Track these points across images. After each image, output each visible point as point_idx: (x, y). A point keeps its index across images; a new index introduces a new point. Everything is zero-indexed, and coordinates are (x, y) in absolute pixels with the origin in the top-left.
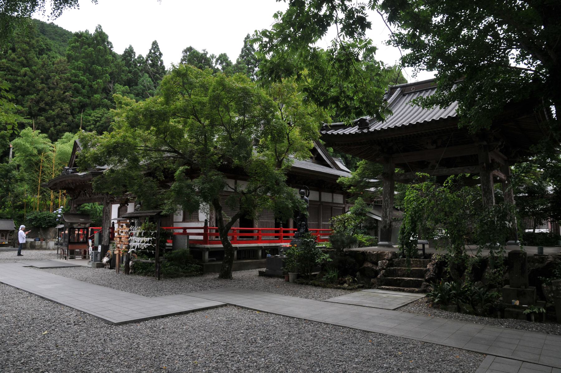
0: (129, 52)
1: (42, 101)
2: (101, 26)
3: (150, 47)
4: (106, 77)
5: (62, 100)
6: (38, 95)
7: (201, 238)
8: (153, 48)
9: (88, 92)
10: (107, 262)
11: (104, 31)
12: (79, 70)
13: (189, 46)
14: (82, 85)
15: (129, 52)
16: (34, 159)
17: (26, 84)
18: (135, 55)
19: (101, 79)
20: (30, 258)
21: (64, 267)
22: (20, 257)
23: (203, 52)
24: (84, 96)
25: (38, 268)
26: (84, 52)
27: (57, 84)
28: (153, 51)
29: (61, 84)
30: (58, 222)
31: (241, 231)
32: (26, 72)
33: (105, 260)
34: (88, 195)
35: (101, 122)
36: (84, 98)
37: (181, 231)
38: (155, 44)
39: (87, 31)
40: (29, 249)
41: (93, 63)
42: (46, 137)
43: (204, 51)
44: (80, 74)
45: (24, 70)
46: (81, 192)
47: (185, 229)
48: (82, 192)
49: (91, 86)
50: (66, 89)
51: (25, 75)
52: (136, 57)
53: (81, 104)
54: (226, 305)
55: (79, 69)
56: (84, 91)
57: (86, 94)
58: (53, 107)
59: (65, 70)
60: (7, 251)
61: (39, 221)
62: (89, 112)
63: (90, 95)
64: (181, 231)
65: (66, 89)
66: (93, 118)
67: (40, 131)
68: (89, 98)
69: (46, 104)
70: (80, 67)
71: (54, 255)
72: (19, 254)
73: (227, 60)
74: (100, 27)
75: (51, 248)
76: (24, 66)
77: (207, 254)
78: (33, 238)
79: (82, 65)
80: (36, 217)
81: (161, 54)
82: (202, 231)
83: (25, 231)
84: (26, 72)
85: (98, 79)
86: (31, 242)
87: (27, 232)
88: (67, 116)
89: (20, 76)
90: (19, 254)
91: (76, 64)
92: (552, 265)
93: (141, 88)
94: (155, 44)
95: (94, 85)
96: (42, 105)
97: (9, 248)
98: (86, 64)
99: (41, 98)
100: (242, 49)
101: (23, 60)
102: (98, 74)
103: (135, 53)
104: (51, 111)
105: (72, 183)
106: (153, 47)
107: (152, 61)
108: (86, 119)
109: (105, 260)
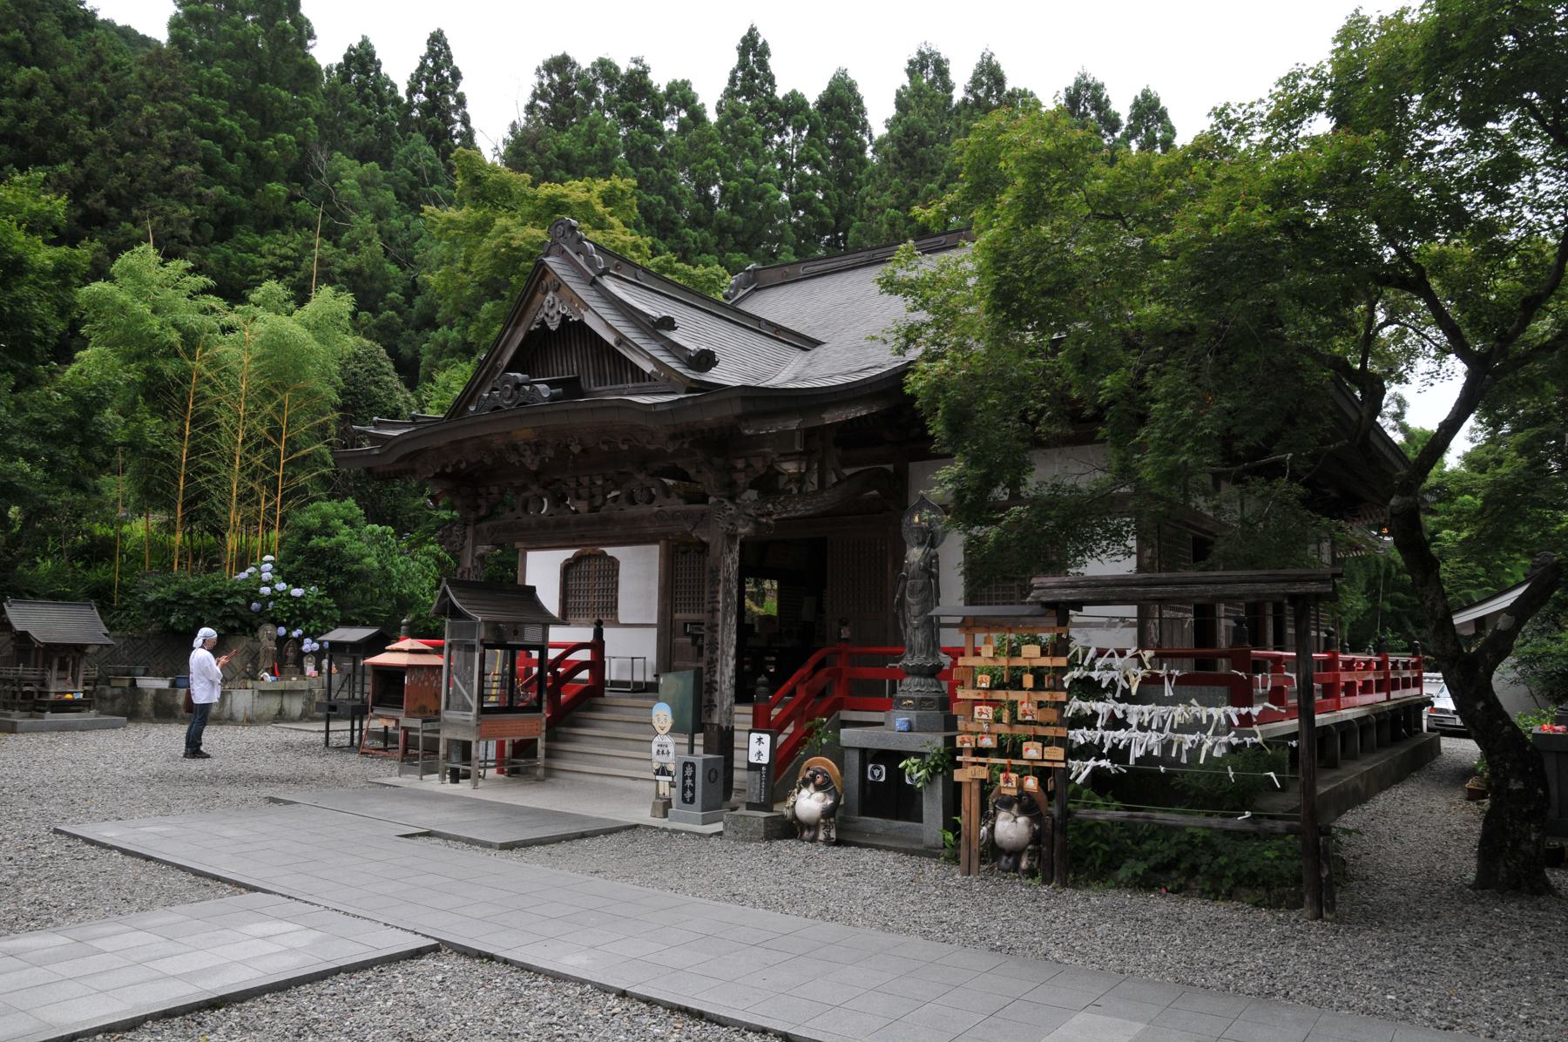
0: (362, 59)
1: (98, 188)
3: (424, 50)
4: (306, 127)
5: (165, 189)
6: (79, 163)
8: (432, 53)
9: (244, 174)
12: (217, 96)
13: (559, 54)
14: (225, 148)
15: (362, 59)
16: (169, 368)
17: (33, 123)
19: (290, 131)
20: (239, 767)
21: (583, 836)
22: (195, 765)
24: (231, 185)
25: (489, 845)
26: (231, 37)
27: (150, 135)
28: (430, 63)
29: (164, 135)
30: (261, 613)
32: (34, 83)
35: (299, 275)
36: (232, 193)
38: (437, 39)
40: (149, 720)
41: (260, 77)
42: (206, 291)
44: (220, 111)
45: (24, 74)
49: (253, 156)
50: (178, 152)
51: (29, 92)
53: (222, 210)
54: (429, 834)
55: (216, 91)
56: (233, 167)
57: (237, 178)
58: (135, 211)
59: (175, 87)
60: (64, 728)
61: (193, 608)
62: (248, 240)
63: (252, 184)
65: (178, 152)
66: (270, 259)
67: (190, 264)
68: (249, 193)
69: (111, 199)
70: (220, 85)
71: (308, 747)
72: (194, 748)
73: (694, 100)
75: (240, 716)
76: (21, 60)
78: (165, 676)
79: (226, 79)
80: (183, 595)
81: (456, 75)
83: (216, 650)
84: (34, 83)
85: (277, 130)
86: (158, 691)
87: (223, 659)
88: (182, 247)
89: (12, 93)
90: (194, 748)
91: (205, 73)
93: (405, 178)
94: (437, 39)
95: (268, 148)
96: (96, 201)
97: (90, 715)
98: (237, 77)
99: (89, 176)
100: (734, 72)
101: (18, 40)
102: (277, 114)
104: (129, 226)
105: (538, 447)
106: (431, 50)
107: (428, 93)
108: (243, 262)
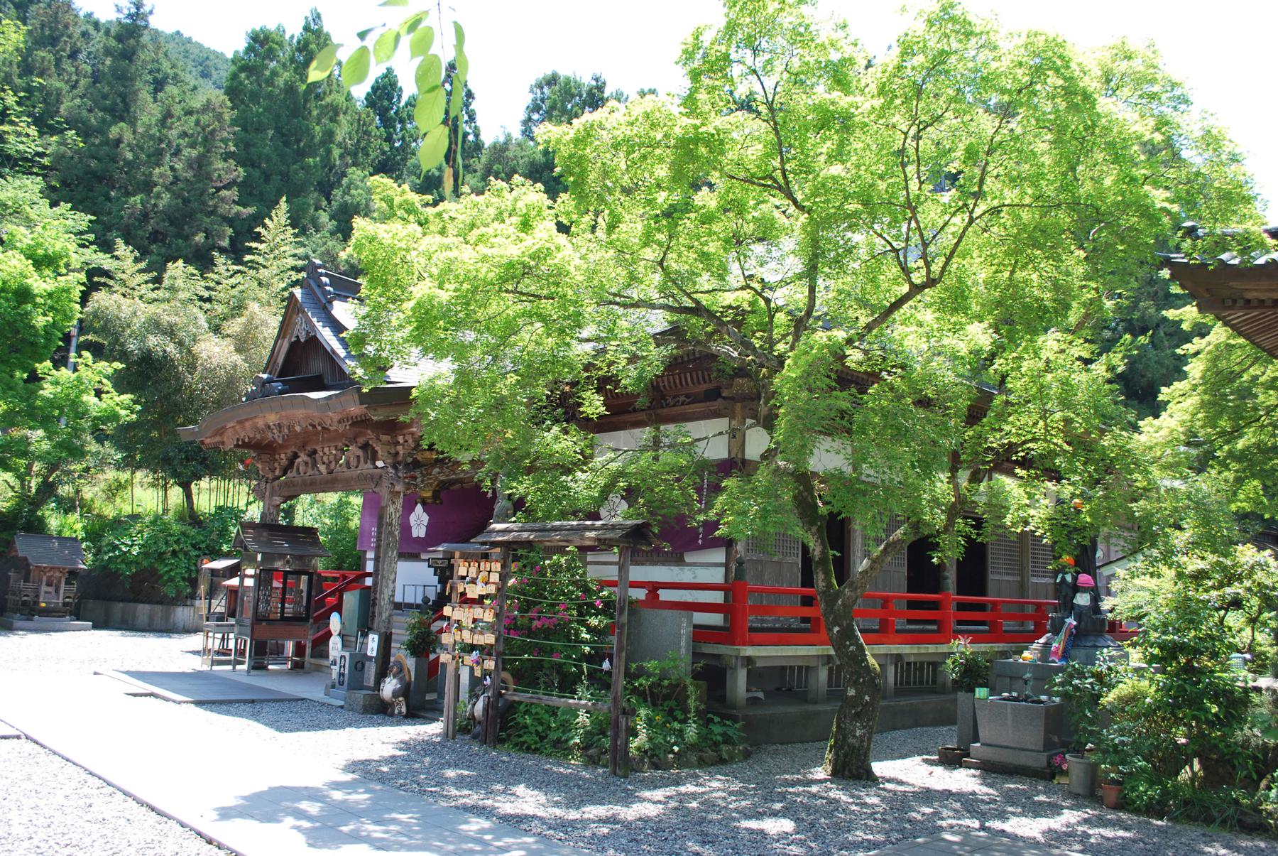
2: (319, 16)
7: (716, 619)
10: (395, 694)
11: (325, 30)
13: (549, 73)
18: (400, 97)
23: (594, 83)
31: (912, 605)
33: (389, 687)
34: (322, 468)
37: (640, 594)
39: (281, 30)
43: (597, 80)
46: (296, 456)
47: (654, 587)
48: (303, 457)
52: (402, 104)
64: (640, 594)
74: (317, 17)
77: (742, 676)
82: (717, 597)
92: (5, 530)
103: (401, 89)
109: (389, 687)
